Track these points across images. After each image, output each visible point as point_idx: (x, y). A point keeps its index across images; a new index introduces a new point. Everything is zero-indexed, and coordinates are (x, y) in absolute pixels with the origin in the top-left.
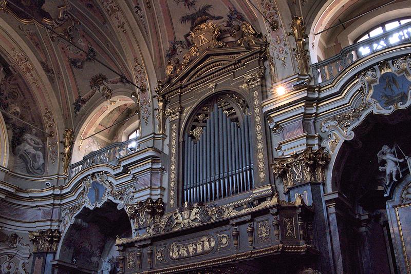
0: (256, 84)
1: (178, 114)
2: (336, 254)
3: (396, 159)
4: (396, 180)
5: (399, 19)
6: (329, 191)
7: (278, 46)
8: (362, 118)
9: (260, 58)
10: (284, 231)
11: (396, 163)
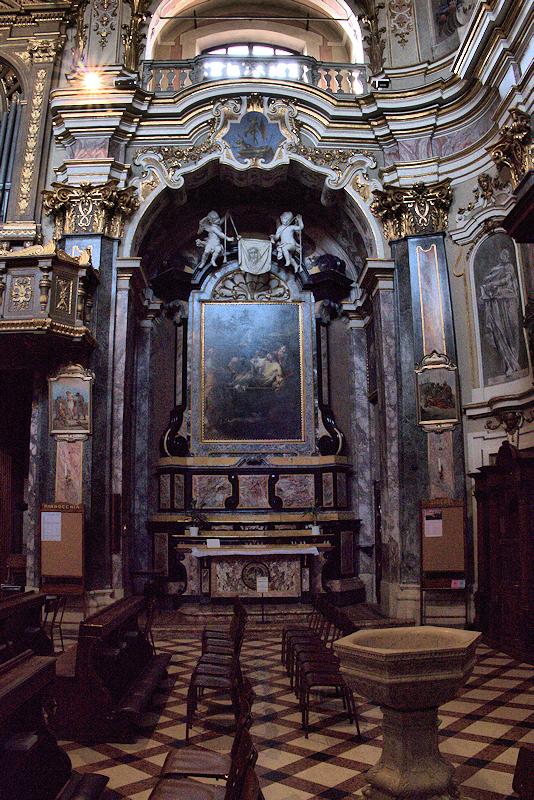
0: (46, 59)
1: (53, 53)
2: (118, 351)
3: (223, 235)
4: (214, 265)
5: (275, 47)
6: (126, 255)
7: (102, 12)
8: (201, 163)
9: (64, 20)
10: (55, 299)
11: (222, 241)
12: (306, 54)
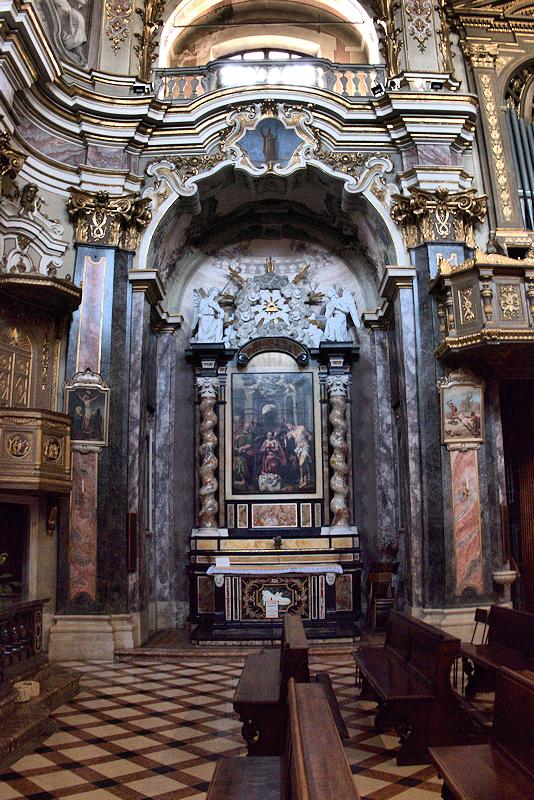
12: (319, 56)
